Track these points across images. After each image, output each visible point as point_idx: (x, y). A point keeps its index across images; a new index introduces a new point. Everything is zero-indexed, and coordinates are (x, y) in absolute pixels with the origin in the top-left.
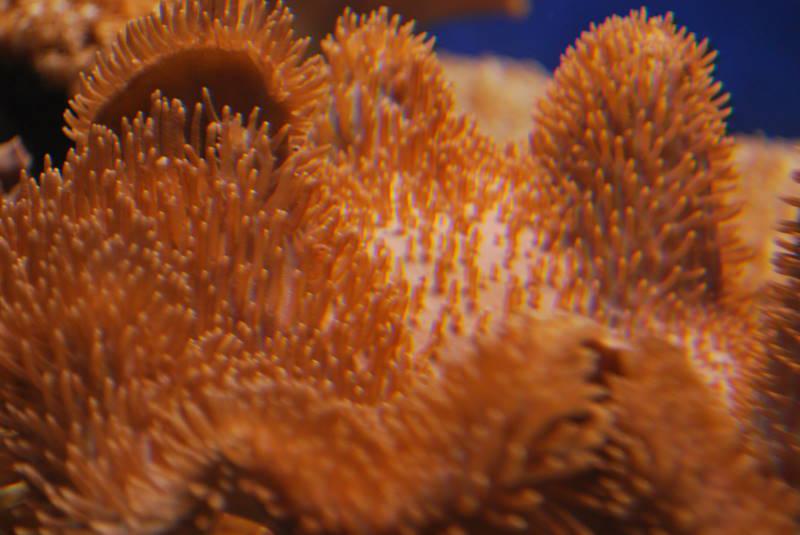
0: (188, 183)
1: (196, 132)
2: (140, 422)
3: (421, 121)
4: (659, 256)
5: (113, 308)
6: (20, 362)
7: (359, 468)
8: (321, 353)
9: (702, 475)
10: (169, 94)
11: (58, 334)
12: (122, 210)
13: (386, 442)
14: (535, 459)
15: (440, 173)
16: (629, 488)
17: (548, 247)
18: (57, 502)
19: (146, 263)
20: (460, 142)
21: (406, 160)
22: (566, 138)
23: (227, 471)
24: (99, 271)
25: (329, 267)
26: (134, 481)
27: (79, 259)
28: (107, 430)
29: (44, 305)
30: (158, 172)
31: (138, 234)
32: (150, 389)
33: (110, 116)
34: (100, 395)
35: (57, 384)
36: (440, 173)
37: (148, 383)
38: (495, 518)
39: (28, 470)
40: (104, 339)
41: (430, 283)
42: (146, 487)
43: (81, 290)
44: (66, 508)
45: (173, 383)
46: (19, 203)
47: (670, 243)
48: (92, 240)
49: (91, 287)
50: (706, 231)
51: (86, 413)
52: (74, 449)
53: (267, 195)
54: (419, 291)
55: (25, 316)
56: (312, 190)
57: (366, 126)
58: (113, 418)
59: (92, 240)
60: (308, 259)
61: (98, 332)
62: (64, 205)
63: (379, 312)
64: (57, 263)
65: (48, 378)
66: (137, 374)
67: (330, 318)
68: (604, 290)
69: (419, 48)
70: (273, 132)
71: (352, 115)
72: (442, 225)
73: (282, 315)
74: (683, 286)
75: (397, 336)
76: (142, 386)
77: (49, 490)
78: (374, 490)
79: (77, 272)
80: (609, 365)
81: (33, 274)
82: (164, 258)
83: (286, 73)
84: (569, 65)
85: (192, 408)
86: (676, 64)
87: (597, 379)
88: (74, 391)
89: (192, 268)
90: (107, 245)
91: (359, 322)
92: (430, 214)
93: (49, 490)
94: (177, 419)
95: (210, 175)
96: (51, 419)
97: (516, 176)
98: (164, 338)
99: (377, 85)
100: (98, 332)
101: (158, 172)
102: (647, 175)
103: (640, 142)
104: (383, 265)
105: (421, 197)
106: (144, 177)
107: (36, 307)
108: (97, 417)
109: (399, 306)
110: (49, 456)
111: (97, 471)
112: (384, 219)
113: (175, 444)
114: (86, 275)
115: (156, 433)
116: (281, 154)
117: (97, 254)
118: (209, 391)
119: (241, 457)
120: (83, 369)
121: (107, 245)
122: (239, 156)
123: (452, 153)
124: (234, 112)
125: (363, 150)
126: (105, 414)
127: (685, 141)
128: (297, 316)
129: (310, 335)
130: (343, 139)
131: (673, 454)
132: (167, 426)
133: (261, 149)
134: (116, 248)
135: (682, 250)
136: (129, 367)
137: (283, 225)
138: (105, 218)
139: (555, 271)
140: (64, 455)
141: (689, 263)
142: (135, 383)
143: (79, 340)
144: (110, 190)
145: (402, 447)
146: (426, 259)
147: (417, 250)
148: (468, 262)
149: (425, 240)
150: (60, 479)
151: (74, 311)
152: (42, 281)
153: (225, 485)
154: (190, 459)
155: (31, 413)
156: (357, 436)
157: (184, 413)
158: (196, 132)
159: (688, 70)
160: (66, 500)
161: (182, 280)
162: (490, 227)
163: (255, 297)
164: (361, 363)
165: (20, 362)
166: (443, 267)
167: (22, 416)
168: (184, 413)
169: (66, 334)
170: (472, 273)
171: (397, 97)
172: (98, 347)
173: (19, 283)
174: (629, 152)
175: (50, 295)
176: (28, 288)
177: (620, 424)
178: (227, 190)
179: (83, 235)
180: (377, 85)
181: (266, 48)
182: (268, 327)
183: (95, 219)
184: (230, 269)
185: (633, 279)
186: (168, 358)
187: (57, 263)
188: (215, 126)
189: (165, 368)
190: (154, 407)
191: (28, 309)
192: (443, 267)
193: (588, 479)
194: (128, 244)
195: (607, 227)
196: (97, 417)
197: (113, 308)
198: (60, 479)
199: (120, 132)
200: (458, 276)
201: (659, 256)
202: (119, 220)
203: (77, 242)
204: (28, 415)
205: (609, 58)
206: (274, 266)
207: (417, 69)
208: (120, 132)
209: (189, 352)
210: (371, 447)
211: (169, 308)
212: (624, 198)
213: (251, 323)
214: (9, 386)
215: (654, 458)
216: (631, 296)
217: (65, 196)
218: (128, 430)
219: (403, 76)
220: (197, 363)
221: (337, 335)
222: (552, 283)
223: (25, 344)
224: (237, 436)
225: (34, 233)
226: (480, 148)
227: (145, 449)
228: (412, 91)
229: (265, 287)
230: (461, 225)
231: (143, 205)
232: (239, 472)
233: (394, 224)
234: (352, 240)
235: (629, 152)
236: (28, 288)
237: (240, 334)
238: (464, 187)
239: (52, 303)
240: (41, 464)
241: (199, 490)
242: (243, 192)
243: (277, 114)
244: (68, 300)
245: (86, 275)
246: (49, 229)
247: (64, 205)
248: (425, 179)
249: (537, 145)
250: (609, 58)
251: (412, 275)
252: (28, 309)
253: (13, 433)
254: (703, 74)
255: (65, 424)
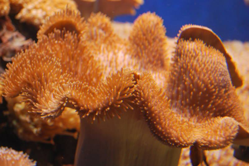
0: (61, 46)
1: (62, 36)
2: (51, 91)
3: (107, 35)
4: (152, 59)
5: (46, 69)
6: (28, 80)
7: (91, 97)
8: (86, 78)
9: (153, 97)
10: (57, 29)
11: (35, 74)
12: (48, 51)
13: (96, 93)
14: (122, 94)
15: (111, 44)
16: (140, 100)
17: (131, 58)
18: (35, 106)
19: (53, 61)
20: (115, 38)
21: (105, 40)
22: (135, 37)
23: (67, 99)
24: (43, 62)
25: (88, 62)
26: (49, 101)
27: (39, 60)
28: (45, 92)
29: (33, 69)
30: (55, 44)
31: (51, 55)
32: (53, 84)
33: (46, 34)
34: (44, 87)
35: (35, 84)
36: (111, 44)
37: (52, 83)
38: (115, 105)
39: (30, 100)
40: (44, 75)
41: (108, 65)
42: (51, 102)
43: (40, 66)
44: (37, 107)
45: (57, 83)
46: (225, 145)
47: (154, 57)
48: (42, 57)
49: (42, 65)
50: (161, 55)
51: (41, 89)
52: (38, 96)
53: (76, 48)
54: (106, 67)
55: (29, 71)
56: (85, 47)
57: (96, 35)
58: (46, 90)
59: (42, 57)
60: (84, 60)
61: (43, 74)
62: (37, 50)
63: (98, 70)
64: (35, 61)
65: (33, 82)
66: (50, 82)
67: (88, 72)
68: (141, 66)
69: (106, 20)
70: (77, 36)
71: (94, 33)
72: (111, 54)
73: (79, 71)
74: (156, 65)
75: (101, 75)
76: (51, 84)
77: (34, 103)
78: (94, 101)
79: (39, 62)
80: (136, 77)
81: (31, 63)
82: (56, 60)
83: (80, 25)
84: (136, 23)
85: (60, 87)
86: (155, 22)
87: (135, 80)
88: (39, 86)
89: (61, 62)
90: (45, 58)
91: (94, 72)
92: (109, 52)
93: (34, 103)
94: (57, 90)
95: (65, 45)
96: (34, 90)
97: (125, 45)
98: (56, 75)
99: (100, 27)
100: (43, 74)
101: (55, 44)
102: (150, 44)
103: (149, 37)
104: (99, 61)
105: (107, 48)
106: (53, 45)
107: (31, 69)
108: (43, 90)
109: (102, 69)
110: (34, 97)
111: (43, 100)
112: (100, 53)
113: (57, 95)
114: (41, 63)
115: (54, 92)
116: (79, 40)
117: (43, 59)
118: (64, 84)
119: (69, 96)
120: (40, 81)
121: (45, 58)
122: (70, 41)
123: (113, 41)
124: (70, 32)
125: (96, 40)
126: (44, 90)
127: (157, 37)
128: (82, 71)
129: (84, 74)
130: (92, 38)
131: (149, 93)
132: (56, 91)
133: (75, 40)
134: (47, 58)
135: (156, 58)
136: (49, 81)
137: (79, 54)
138: (45, 53)
139: (132, 63)
140: (37, 97)
141: (158, 60)
142: (50, 83)
143: (39, 75)
144: (46, 47)
145: (99, 94)
146: (108, 60)
147: (106, 59)
148: (116, 61)
149: (108, 57)
150: (36, 101)
151: (38, 70)
152: (32, 64)
153: (66, 102)
154: (60, 97)
155: (30, 89)
156: (90, 91)
157: (59, 89)
158: (62, 36)
159: (158, 24)
160: (37, 105)
161: (59, 64)
162: (120, 55)
163: (74, 67)
164: (94, 80)
165: (28, 80)
166: (111, 62)
167: (29, 90)
168: (59, 89)
169: (37, 74)
170: (116, 63)
171: (103, 29)
172: (43, 76)
173: (28, 65)
174: (146, 39)
175: (34, 67)
176: (30, 66)
177: (138, 87)
178: (68, 47)
179: (40, 56)
180: (100, 27)
181: (75, 20)
182: (76, 73)
183: (43, 53)
184: (69, 62)
185: (147, 64)
186: (56, 79)
187: (35, 61)
188: (66, 35)
189: (56, 80)
190: (53, 88)
191: (30, 69)
192: (111, 62)
193: (133, 98)
194: (49, 57)
195: (142, 53)
196: (43, 90)
197: (46, 69)
198: (36, 101)
199: (48, 36)
200: (114, 64)
201: (152, 59)
202: (47, 53)
203: (39, 57)
204: (30, 90)
205: (143, 21)
206: (77, 61)
207: (106, 24)
208: (48, 36)
209: (60, 77)
210: (93, 94)
211: (57, 69)
212: (146, 48)
213: (73, 72)
214: (26, 84)
215: (144, 94)
216: (147, 67)
217: (38, 49)
218: (49, 92)
219: (104, 26)
220: (62, 79)
221: (90, 75)
222: (132, 64)
223: (29, 76)
224: (68, 93)
225: (31, 55)
226: (119, 40)
227: (52, 95)
228: (105, 29)
229: (76, 65)
230: (115, 54)
231: (53, 51)
232: (69, 99)
233: (102, 54)
234: (92, 57)
235: (146, 39)
236: (30, 66)
237: (70, 74)
238: (115, 47)
239: (34, 68)
240: (32, 99)
241: (61, 103)
242: (72, 47)
243: (78, 33)
244: (37, 68)
245: (41, 63)
246: (34, 55)
247: (37, 50)
248: (108, 45)
249: (130, 39)
250: (143, 21)
251: (105, 64)
252: (30, 69)
253: (27, 93)
254: (161, 25)
255: (37, 91)
